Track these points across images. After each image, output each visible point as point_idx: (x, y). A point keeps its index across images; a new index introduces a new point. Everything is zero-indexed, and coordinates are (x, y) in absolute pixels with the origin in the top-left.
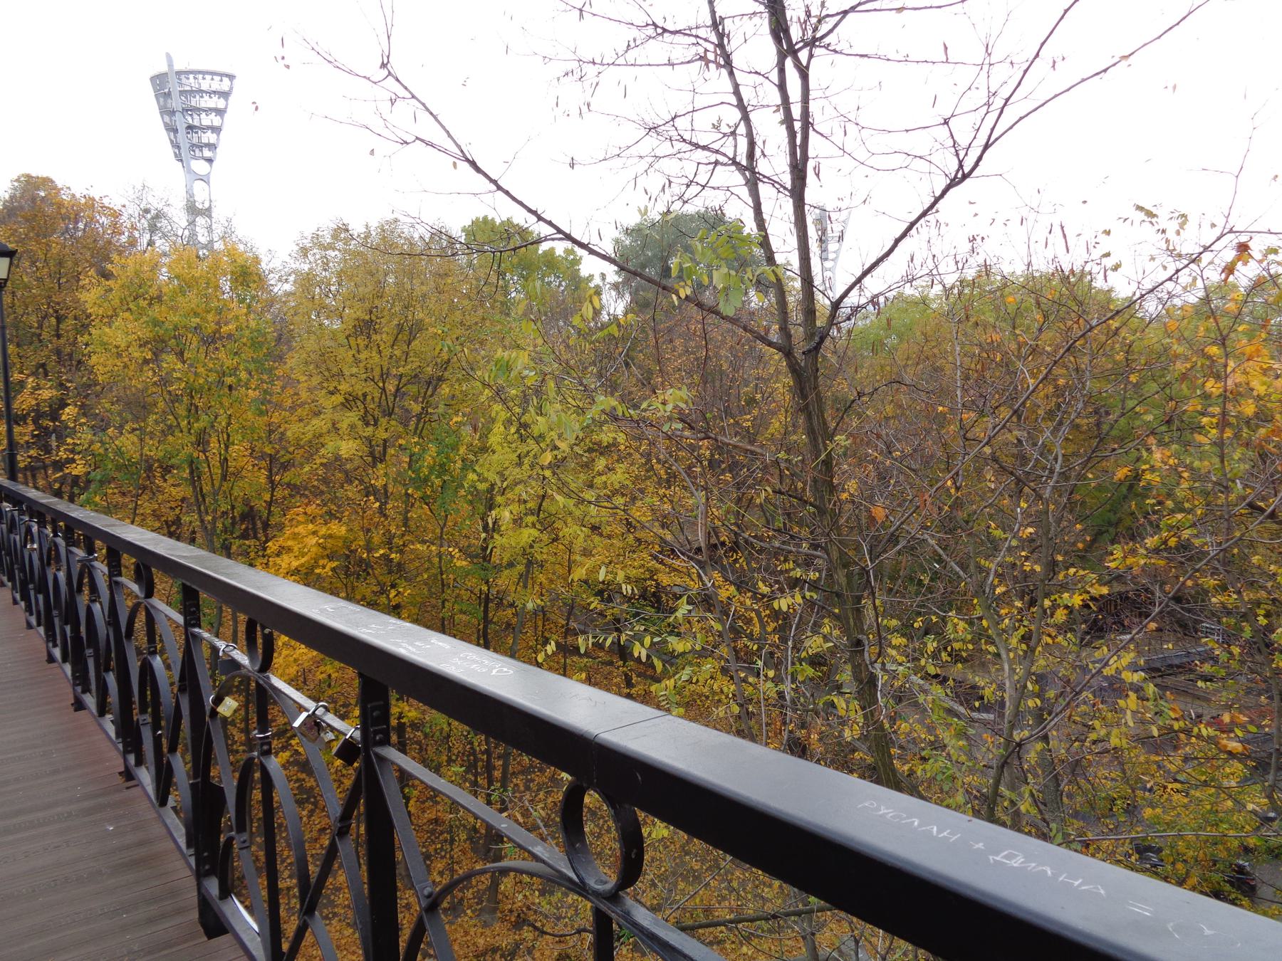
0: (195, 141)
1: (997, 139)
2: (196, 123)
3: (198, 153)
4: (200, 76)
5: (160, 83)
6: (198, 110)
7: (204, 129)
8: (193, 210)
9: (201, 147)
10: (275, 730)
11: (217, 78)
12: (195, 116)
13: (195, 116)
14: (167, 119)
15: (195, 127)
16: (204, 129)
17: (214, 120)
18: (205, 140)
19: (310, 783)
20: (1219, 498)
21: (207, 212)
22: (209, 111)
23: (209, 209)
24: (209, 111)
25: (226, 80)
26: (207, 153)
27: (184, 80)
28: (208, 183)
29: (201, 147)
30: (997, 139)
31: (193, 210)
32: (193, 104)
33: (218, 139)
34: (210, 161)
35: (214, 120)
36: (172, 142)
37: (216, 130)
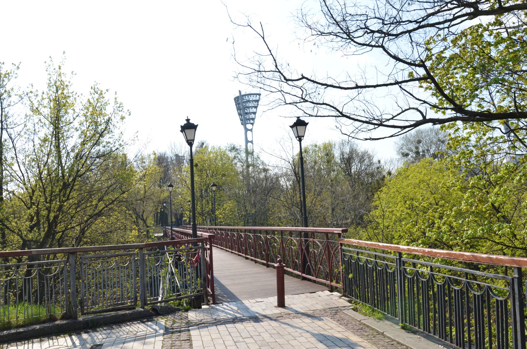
0: (248, 118)
1: (426, 113)
2: (248, 112)
3: (249, 122)
4: (250, 96)
5: (237, 99)
6: (249, 107)
7: (250, 113)
8: (247, 153)
9: (249, 119)
10: (53, 151)
11: (255, 96)
12: (248, 109)
13: (248, 109)
14: (239, 111)
15: (248, 113)
16: (250, 113)
17: (254, 110)
18: (251, 117)
19: (74, 102)
20: (466, 227)
21: (252, 153)
22: (252, 107)
23: (253, 152)
24: (252, 107)
25: (258, 96)
26: (252, 122)
27: (244, 98)
28: (252, 132)
29: (249, 119)
30: (426, 113)
31: (247, 153)
32: (247, 105)
33: (255, 117)
34: (252, 124)
35: (254, 110)
36: (240, 119)
37: (255, 113)
